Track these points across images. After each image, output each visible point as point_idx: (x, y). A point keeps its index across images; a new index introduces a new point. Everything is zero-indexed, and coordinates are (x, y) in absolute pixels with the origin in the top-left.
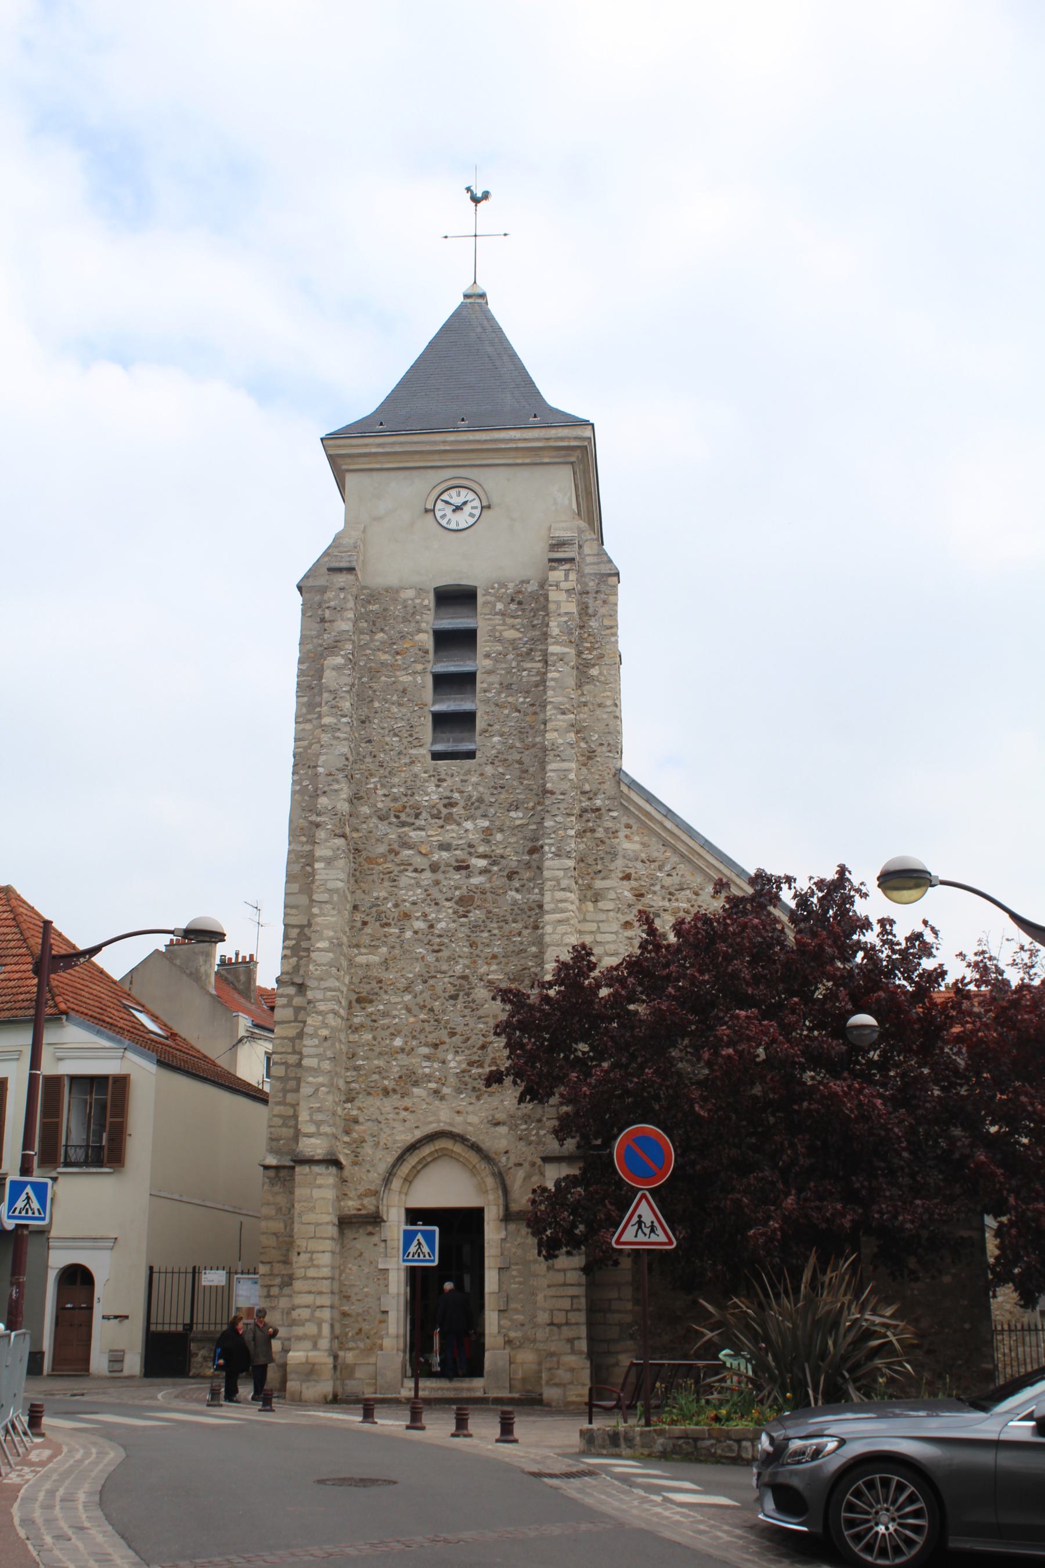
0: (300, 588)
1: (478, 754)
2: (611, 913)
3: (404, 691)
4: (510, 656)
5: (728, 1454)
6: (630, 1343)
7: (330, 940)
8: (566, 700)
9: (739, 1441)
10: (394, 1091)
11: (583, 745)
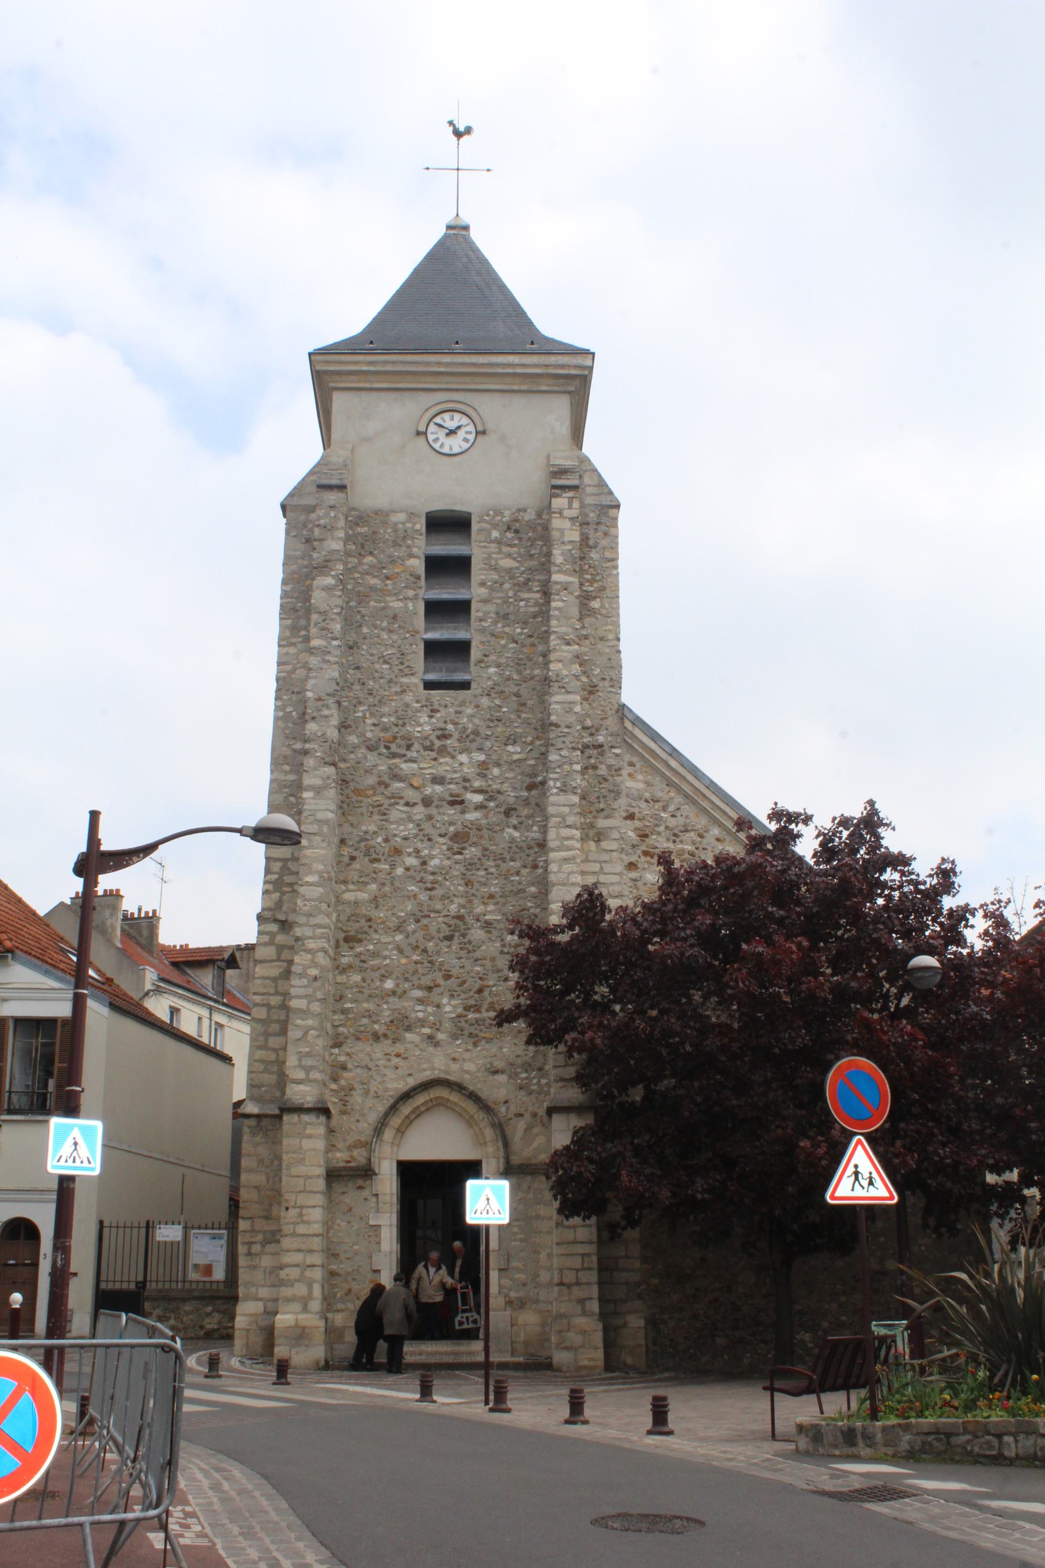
0: (284, 507)
1: (473, 685)
2: (615, 854)
3: (395, 617)
4: (507, 586)
6: (638, 1304)
7: (320, 874)
8: (570, 630)
9: (999, 1436)
10: (385, 1036)
11: (584, 679)
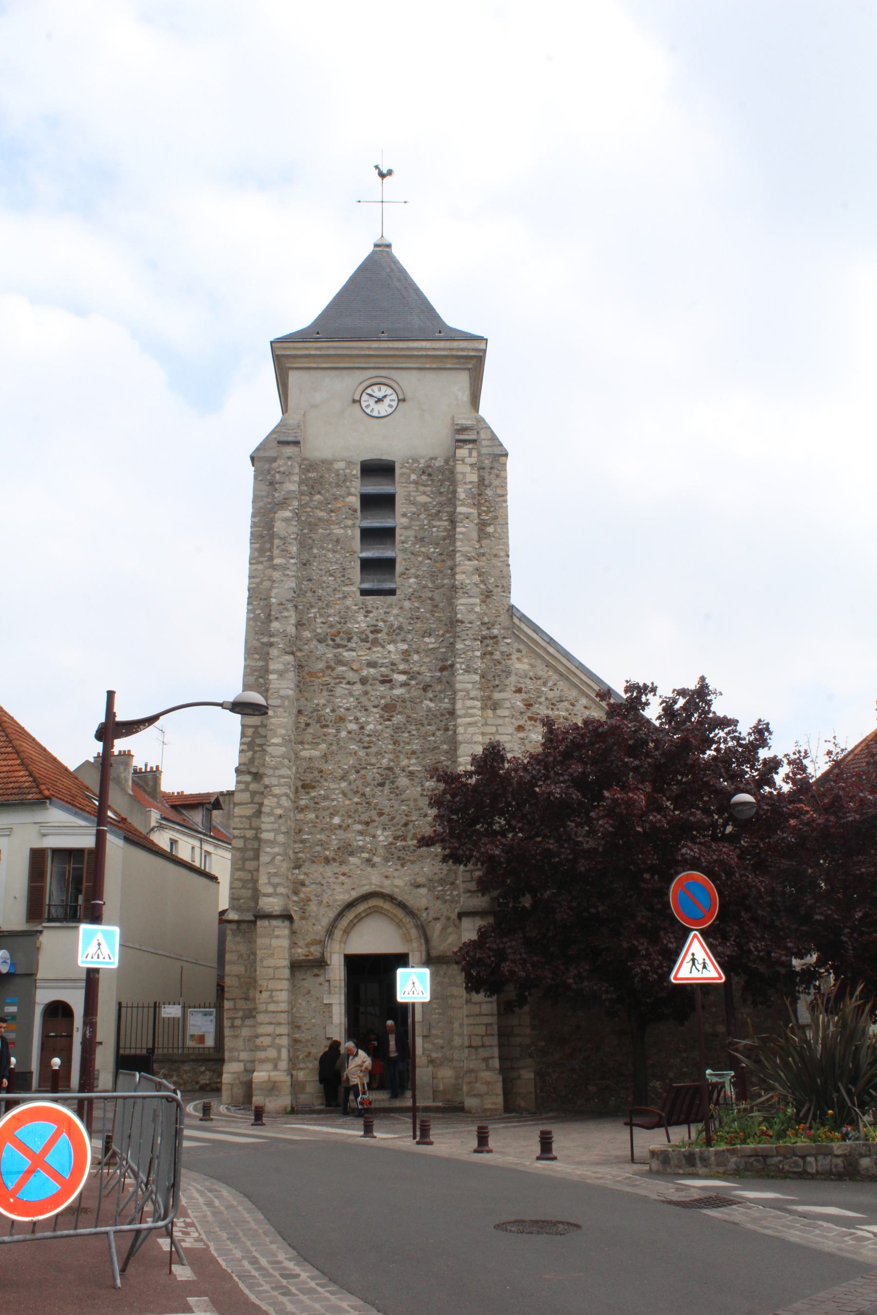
0: (252, 458)
1: (398, 592)
2: (507, 719)
3: (338, 541)
4: (423, 516)
5: (794, 1170)
8: (471, 549)
9: (803, 1157)
11: (482, 586)
